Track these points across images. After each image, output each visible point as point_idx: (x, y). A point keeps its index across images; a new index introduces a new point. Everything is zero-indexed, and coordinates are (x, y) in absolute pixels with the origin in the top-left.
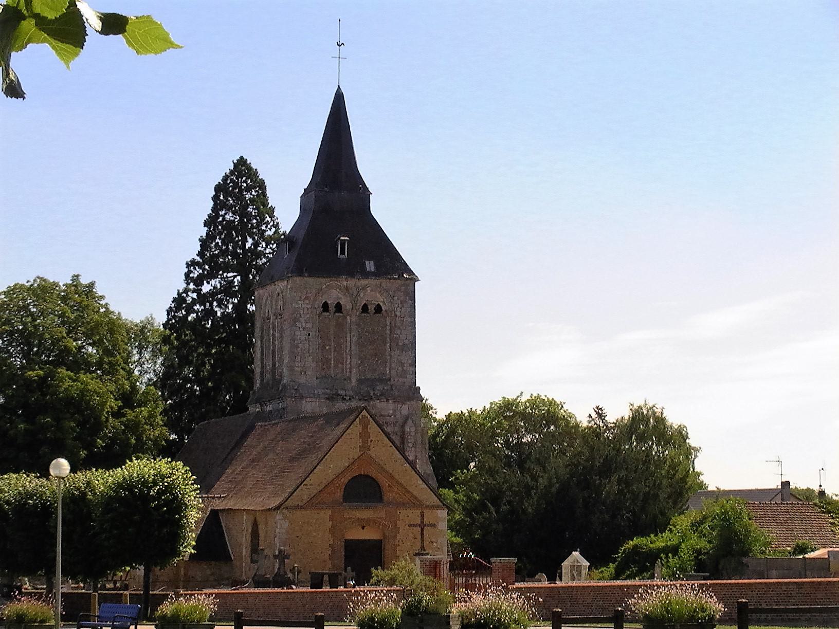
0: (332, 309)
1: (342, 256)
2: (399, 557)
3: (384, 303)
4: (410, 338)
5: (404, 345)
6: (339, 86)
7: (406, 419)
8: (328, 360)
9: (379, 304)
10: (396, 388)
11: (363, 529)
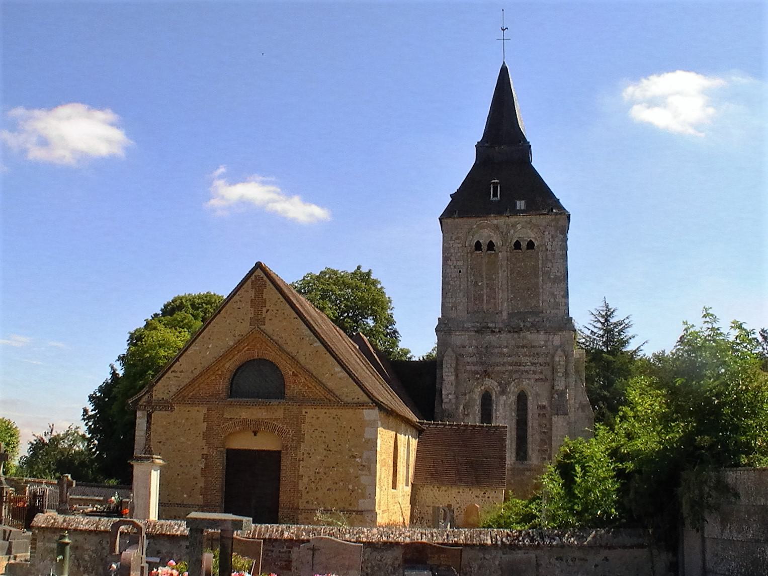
0: (484, 247)
1: (495, 199)
2: (302, 476)
5: (556, 277)
6: (504, 62)
9: (531, 240)
11: (255, 435)
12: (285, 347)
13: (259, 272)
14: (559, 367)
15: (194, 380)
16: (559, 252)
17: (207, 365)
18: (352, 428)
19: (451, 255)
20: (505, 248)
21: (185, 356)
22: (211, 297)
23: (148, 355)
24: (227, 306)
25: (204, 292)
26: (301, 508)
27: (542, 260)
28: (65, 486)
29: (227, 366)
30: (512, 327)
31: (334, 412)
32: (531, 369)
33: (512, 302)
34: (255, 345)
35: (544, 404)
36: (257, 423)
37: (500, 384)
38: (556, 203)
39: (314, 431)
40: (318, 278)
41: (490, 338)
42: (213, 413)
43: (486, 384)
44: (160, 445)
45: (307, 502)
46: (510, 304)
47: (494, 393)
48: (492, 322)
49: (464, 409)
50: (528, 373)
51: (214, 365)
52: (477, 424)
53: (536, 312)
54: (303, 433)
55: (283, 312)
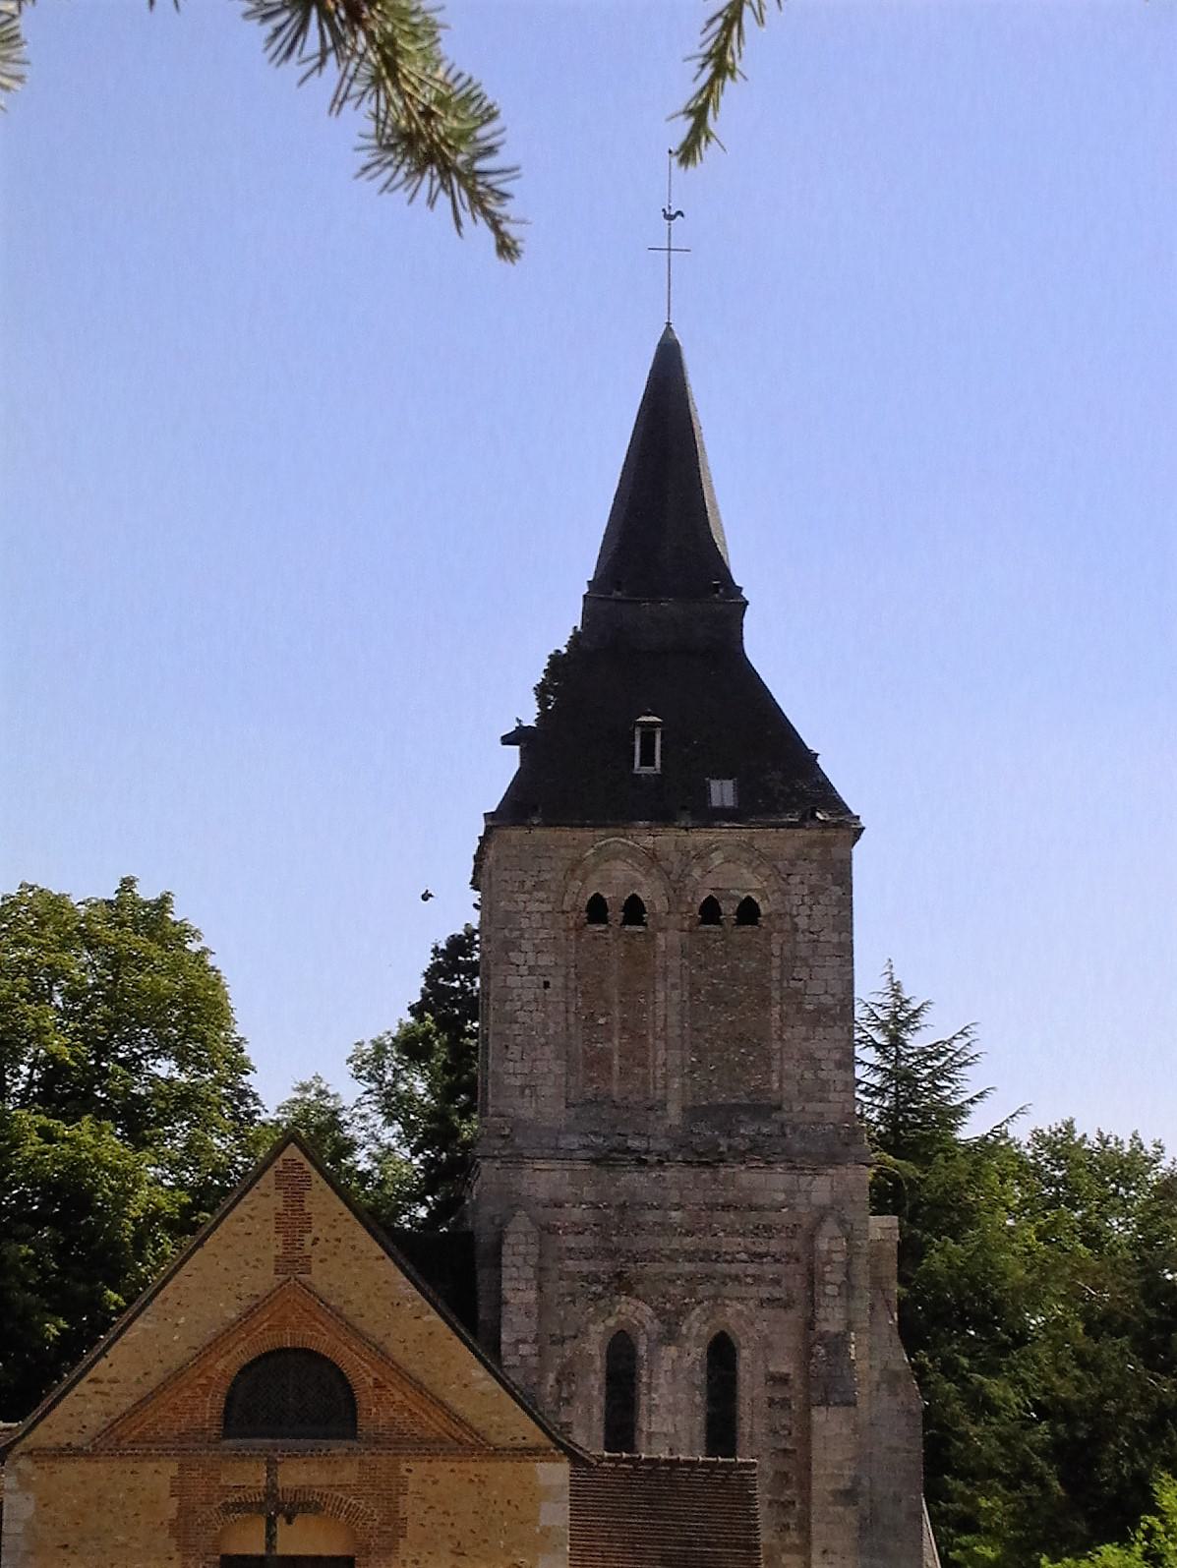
0: (616, 915)
3: (765, 897)
4: (837, 988)
5: (822, 1010)
6: (669, 324)
7: (822, 1214)
10: (794, 1129)
12: (358, 1323)
14: (828, 1268)
15: (143, 1402)
17: (175, 1367)
18: (512, 1503)
19: (522, 936)
20: (675, 918)
21: (123, 1344)
27: (781, 957)
29: (220, 1366)
31: (471, 1468)
36: (351, 1509)
37: (660, 1313)
38: (827, 796)
41: (635, 1181)
42: (194, 1474)
43: (620, 1312)
47: (643, 1339)
48: (639, 1135)
49: (558, 1381)
50: (740, 1281)
52: (701, 1459)
53: (763, 1109)
54: (401, 1516)
55: (351, 1243)
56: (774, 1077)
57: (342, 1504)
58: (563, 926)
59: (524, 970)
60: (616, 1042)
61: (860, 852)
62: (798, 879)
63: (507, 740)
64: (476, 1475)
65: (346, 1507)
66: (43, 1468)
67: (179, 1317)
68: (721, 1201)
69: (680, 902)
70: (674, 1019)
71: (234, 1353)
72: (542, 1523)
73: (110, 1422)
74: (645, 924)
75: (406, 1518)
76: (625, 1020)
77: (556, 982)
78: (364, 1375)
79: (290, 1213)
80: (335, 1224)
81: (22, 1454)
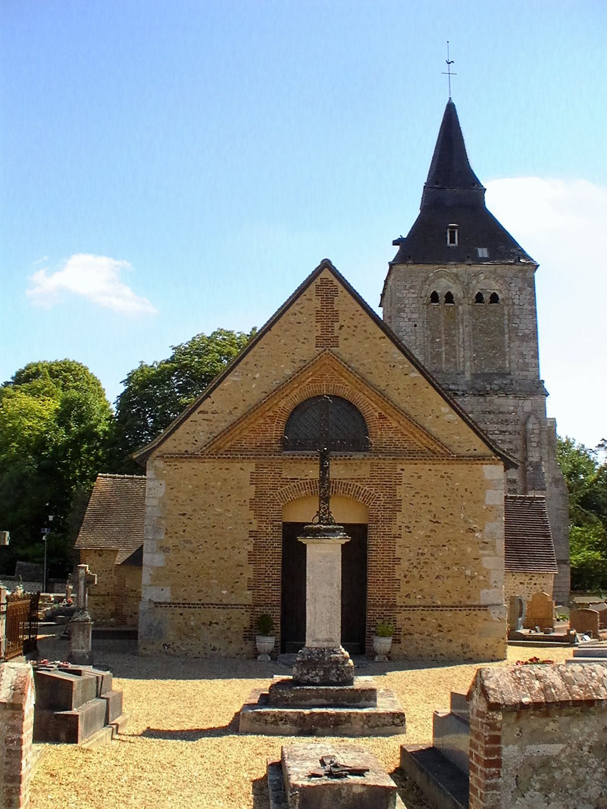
0: (442, 299)
1: (453, 245)
3: (501, 292)
4: (531, 326)
5: (525, 335)
8: (439, 354)
12: (369, 377)
13: (326, 274)
14: (532, 436)
15: (233, 425)
16: (527, 306)
18: (468, 490)
19: (405, 307)
22: (71, 364)
23: (10, 425)
24: (281, 320)
25: (60, 358)
26: (398, 604)
28: (82, 583)
29: (282, 404)
30: (477, 390)
31: (443, 468)
32: (499, 438)
33: (475, 362)
34: (322, 375)
35: (514, 477)
36: (366, 493)
38: (522, 254)
39: (414, 496)
40: (211, 339)
44: (184, 519)
45: (407, 596)
46: (473, 363)
51: (265, 402)
53: (503, 375)
55: (364, 328)
56: (507, 362)
57: (360, 490)
58: (422, 303)
59: (406, 320)
60: (444, 348)
61: (537, 274)
62: (514, 285)
63: (395, 243)
64: (445, 473)
65: (362, 492)
66: (170, 466)
67: (256, 374)
68: (488, 410)
69: (468, 293)
70: (466, 339)
71: (291, 396)
72: (487, 503)
73: (212, 438)
74: (454, 303)
75: (401, 500)
76: (447, 340)
77: (419, 324)
78: (373, 411)
79: (325, 310)
80: (353, 317)
81: (157, 457)
